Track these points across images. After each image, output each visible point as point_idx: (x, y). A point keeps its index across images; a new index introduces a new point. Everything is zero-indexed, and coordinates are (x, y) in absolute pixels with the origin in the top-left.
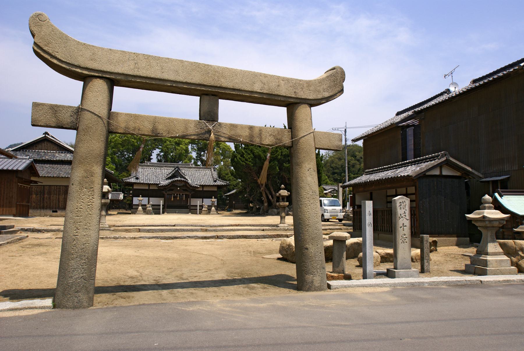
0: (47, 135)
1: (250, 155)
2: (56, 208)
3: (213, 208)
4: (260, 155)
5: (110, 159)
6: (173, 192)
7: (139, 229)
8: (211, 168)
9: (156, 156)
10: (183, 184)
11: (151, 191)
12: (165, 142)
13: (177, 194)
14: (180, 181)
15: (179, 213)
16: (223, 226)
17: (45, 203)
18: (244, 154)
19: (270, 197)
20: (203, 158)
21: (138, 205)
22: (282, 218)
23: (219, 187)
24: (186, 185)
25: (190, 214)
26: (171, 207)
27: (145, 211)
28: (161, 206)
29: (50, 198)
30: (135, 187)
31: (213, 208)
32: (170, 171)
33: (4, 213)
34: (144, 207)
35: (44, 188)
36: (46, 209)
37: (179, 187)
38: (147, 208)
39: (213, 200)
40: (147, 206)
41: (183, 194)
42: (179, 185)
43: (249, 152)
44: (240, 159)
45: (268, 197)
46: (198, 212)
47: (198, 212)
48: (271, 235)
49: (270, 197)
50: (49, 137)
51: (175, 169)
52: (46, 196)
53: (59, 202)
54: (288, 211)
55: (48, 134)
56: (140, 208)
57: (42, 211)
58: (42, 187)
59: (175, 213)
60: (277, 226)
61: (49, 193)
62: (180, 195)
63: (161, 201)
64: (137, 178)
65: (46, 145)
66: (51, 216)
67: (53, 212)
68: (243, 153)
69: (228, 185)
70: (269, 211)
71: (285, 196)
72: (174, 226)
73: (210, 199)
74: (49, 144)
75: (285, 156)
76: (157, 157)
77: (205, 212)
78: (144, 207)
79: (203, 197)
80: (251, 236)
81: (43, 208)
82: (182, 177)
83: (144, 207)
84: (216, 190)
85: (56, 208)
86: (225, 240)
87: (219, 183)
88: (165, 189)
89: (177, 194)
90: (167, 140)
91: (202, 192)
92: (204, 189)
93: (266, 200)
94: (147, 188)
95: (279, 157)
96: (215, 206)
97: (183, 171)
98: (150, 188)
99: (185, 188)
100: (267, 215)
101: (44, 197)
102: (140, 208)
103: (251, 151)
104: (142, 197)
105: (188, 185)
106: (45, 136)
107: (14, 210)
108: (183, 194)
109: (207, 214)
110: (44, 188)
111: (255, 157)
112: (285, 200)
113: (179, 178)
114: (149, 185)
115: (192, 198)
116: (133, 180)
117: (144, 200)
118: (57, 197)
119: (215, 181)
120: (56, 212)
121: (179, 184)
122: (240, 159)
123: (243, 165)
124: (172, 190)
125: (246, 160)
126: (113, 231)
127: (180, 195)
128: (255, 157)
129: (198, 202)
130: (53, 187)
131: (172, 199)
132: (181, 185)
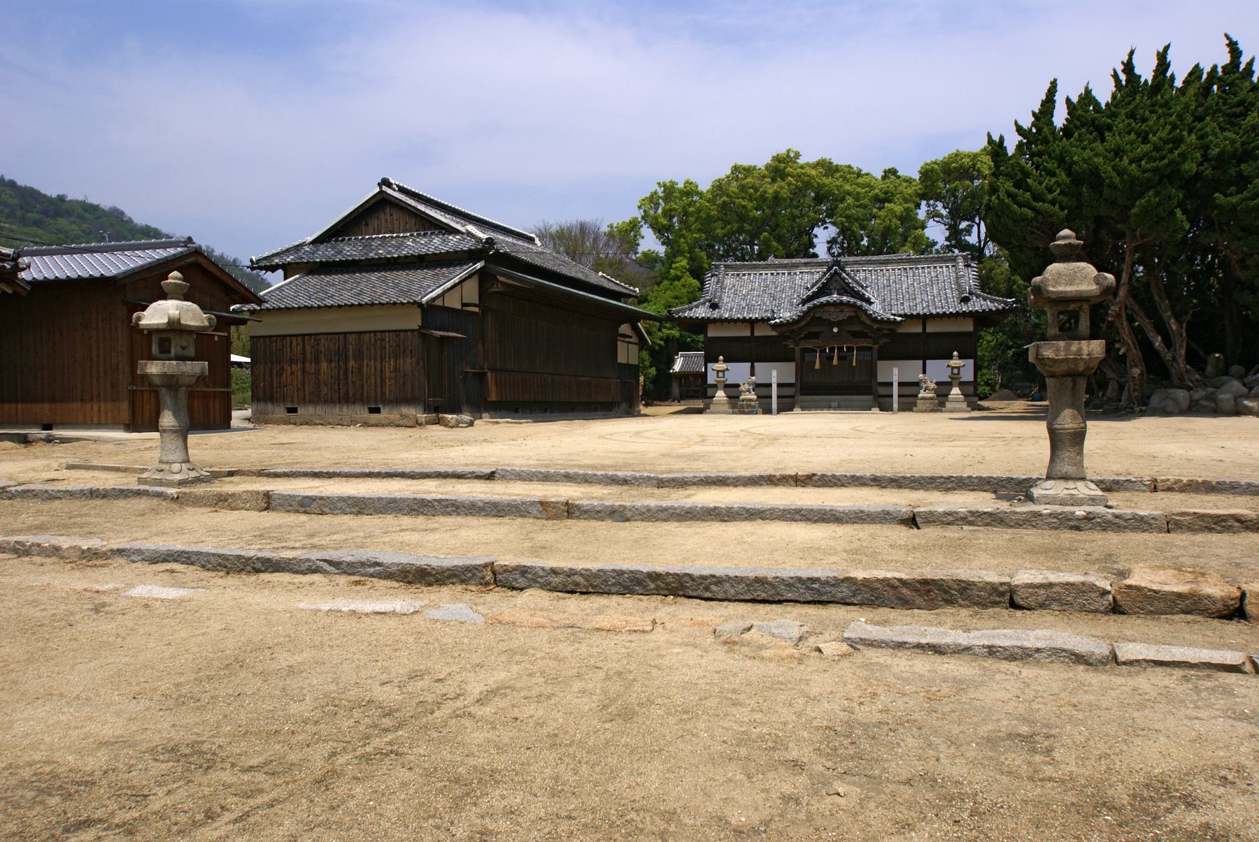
0: (384, 188)
1: (1053, 175)
2: (376, 402)
3: (956, 391)
4: (1095, 171)
5: (684, 263)
6: (819, 342)
7: (267, 495)
8: (954, 259)
9: (826, 246)
10: (848, 313)
11: (754, 342)
12: (843, 200)
13: (832, 350)
14: (835, 304)
15: (840, 407)
16: (682, 483)
17: (351, 386)
18: (1027, 175)
19: (1158, 342)
20: (967, 238)
21: (715, 386)
22: (1066, 443)
23: (982, 319)
24: (857, 317)
25: (876, 410)
26: (810, 391)
27: (737, 405)
28: (774, 387)
29: (360, 369)
30: (711, 334)
31: (956, 391)
32: (817, 277)
33: (103, 420)
34: (733, 390)
35: (345, 339)
36: (354, 403)
37: (838, 324)
38: (741, 393)
39: (955, 362)
40: (742, 388)
41: (850, 349)
42: (833, 318)
43: (1052, 165)
44: (1009, 194)
45: (1145, 345)
46: (895, 406)
47: (895, 406)
48: (866, 583)
49: (1158, 342)
50: (389, 191)
51: (829, 270)
52: (351, 363)
53: (383, 380)
54: (1238, 397)
55: (389, 185)
56: (720, 394)
57: (345, 409)
58: (342, 337)
59: (829, 408)
60: (1020, 488)
61: (359, 356)
62: (841, 349)
63: (774, 373)
64: (714, 306)
65: (388, 216)
66: (366, 425)
67: (372, 411)
68: (1023, 170)
69: (1012, 310)
70: (1155, 400)
71: (1080, 299)
72: (490, 477)
73: (945, 362)
74: (396, 215)
75: (1222, 161)
76: (829, 249)
77: (928, 405)
78: (733, 392)
79: (925, 356)
80: (719, 581)
81: (347, 400)
82: (846, 289)
83: (733, 390)
84: (971, 329)
85: (376, 402)
86: (533, 598)
87: (977, 305)
88: (792, 331)
89: (832, 350)
90: (849, 194)
91: (919, 339)
92: (929, 329)
93: (1135, 353)
94: (748, 334)
95: (1190, 167)
96: (962, 385)
97: (860, 276)
98: (757, 334)
99: (857, 328)
100: (1142, 414)
101: (346, 368)
102: (720, 394)
103: (1061, 160)
104: (725, 361)
105: (864, 318)
106: (381, 192)
107: (125, 414)
108: (850, 349)
109: (932, 411)
110: (345, 339)
111: (1077, 180)
112: (1084, 324)
113: (835, 297)
114: (752, 323)
115: (882, 358)
116: (701, 312)
117: (738, 372)
118: (378, 364)
119: (965, 300)
120: (377, 411)
121: (834, 316)
122: (1009, 194)
123: (1024, 219)
124: (816, 335)
125: (1038, 197)
126: (176, 499)
127: (841, 349)
128: (1077, 180)
129: (894, 373)
130: (366, 337)
131: (817, 366)
132: (842, 317)
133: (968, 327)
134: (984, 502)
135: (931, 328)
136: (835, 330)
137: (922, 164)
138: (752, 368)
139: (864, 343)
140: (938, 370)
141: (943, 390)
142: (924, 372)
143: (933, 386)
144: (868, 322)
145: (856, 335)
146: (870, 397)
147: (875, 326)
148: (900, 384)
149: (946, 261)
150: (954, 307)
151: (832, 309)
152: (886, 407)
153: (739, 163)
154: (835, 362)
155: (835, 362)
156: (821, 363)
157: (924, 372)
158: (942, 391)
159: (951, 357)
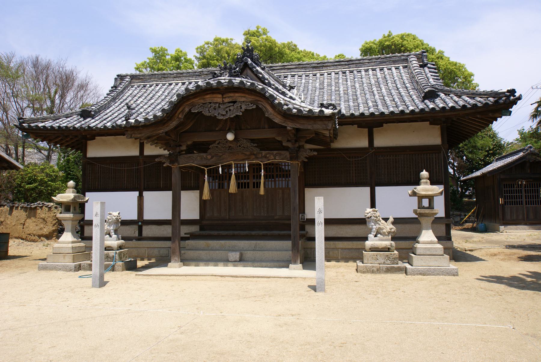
15: (242, 260)
42: (221, 114)
73: (409, 189)
99: (267, 134)
105: (270, 112)
132: (235, 112)
133: (431, 137)
134: (295, 67)
135: (384, 140)
136: (230, 137)
137: (363, 43)
138: (141, 198)
139: (275, 158)
140: (396, 201)
141: (407, 230)
142: (373, 205)
143: (388, 227)
144: (278, 120)
145: (265, 145)
146: (288, 244)
147: (290, 125)
148: (328, 222)
149: (394, 62)
150: (414, 103)
151: (218, 98)
152: (308, 260)
153: (219, 36)
154: (233, 187)
155: (233, 187)
156: (211, 191)
157: (373, 205)
158: (405, 234)
159: (417, 182)
